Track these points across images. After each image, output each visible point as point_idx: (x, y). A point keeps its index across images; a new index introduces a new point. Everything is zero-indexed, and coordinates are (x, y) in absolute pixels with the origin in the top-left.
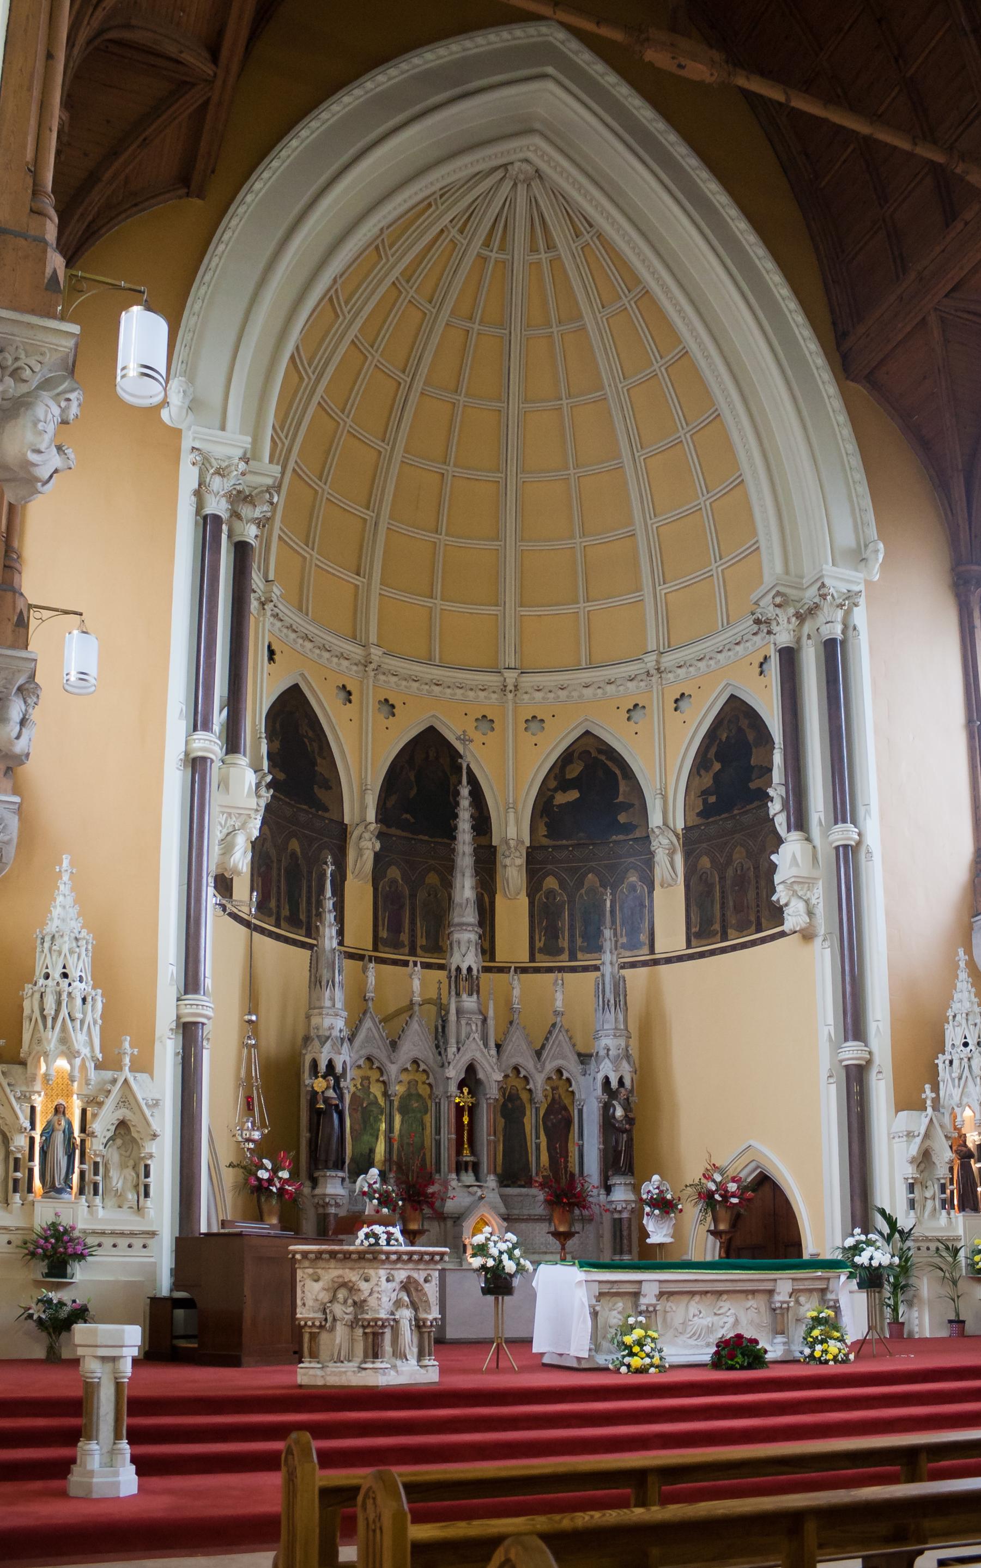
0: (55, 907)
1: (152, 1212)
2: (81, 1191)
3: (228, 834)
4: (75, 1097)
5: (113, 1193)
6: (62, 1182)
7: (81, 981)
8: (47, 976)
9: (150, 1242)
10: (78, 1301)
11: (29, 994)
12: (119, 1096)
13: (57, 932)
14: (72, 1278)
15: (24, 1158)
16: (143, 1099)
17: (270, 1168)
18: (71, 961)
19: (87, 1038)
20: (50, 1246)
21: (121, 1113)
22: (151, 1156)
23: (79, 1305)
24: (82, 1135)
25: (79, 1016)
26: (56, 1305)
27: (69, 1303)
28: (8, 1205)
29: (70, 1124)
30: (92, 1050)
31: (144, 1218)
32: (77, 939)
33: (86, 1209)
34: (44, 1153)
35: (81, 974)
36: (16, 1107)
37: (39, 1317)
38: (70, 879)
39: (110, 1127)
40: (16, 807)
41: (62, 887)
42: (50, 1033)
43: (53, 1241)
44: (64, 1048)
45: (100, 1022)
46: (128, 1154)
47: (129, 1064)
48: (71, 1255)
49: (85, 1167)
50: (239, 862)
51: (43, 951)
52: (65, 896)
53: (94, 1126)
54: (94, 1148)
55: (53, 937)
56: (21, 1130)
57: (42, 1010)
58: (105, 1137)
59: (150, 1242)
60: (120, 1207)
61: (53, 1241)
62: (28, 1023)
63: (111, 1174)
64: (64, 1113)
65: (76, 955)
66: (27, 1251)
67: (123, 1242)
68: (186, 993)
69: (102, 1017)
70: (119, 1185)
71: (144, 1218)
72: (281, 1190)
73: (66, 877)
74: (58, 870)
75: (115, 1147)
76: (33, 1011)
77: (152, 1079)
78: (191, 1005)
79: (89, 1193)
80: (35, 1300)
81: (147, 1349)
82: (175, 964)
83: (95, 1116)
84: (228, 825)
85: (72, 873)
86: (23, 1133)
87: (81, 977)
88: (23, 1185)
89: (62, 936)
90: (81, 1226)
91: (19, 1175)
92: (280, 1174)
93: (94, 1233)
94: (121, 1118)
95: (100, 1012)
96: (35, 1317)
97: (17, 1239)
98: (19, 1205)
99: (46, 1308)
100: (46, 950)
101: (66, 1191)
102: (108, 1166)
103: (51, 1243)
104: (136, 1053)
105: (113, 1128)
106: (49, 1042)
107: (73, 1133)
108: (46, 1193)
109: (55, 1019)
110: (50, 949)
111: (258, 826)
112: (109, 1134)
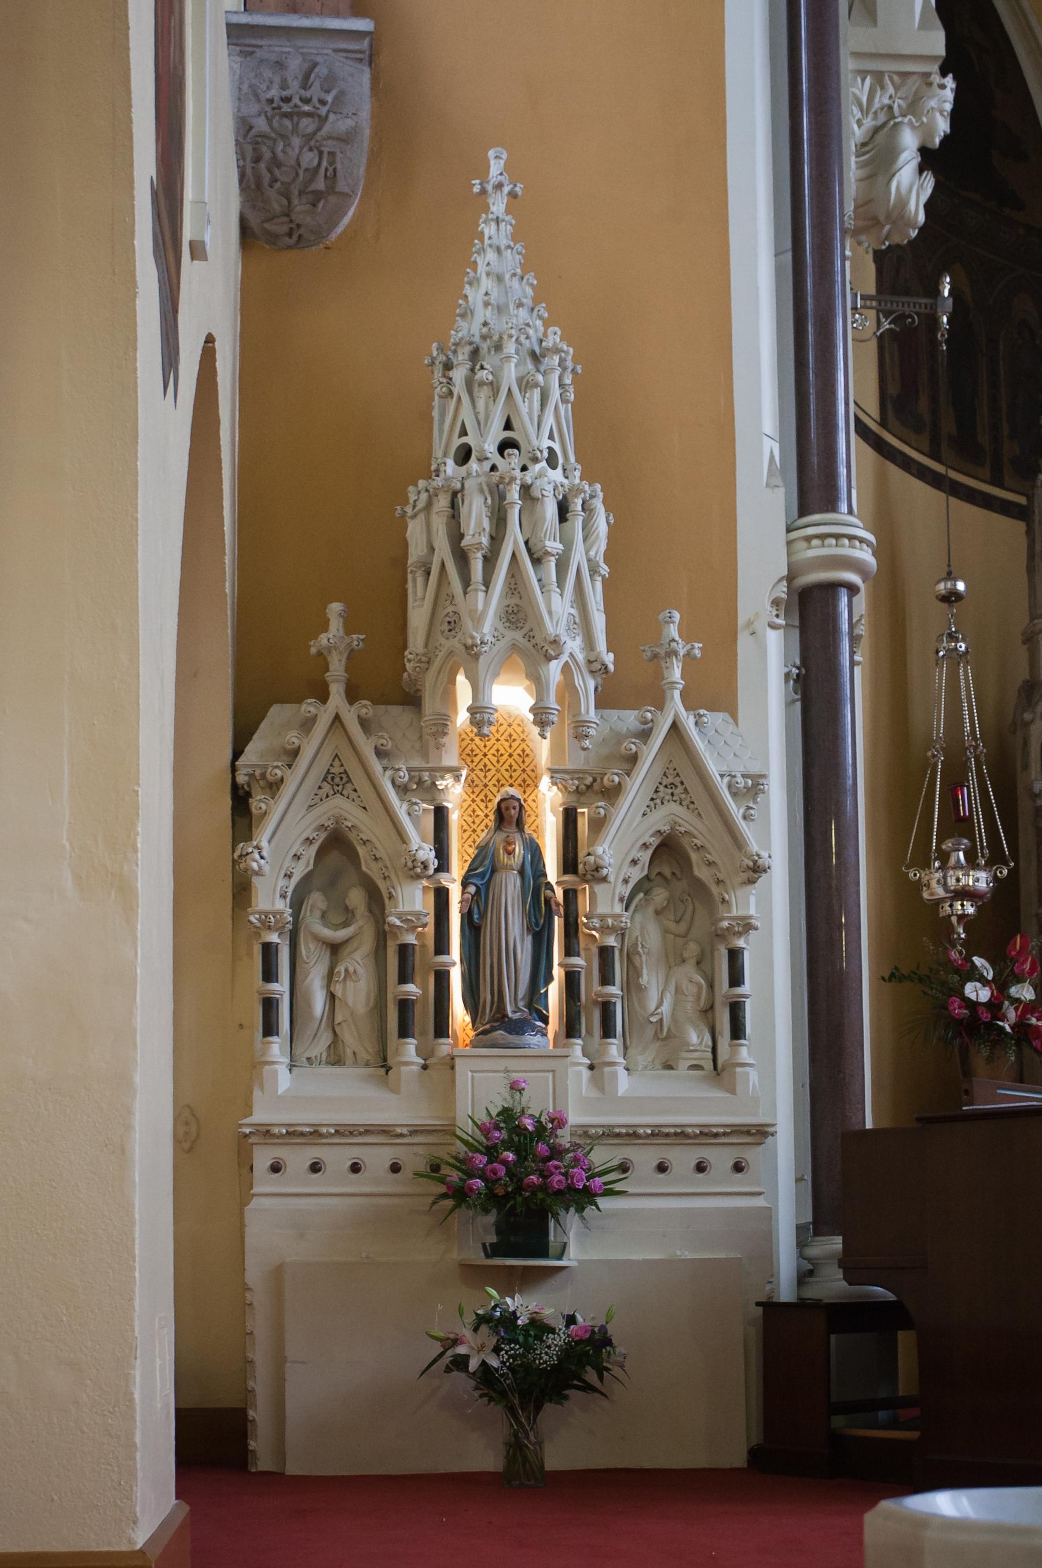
0: (474, 282)
1: (753, 1075)
2: (571, 1029)
3: (876, 130)
4: (545, 781)
5: (650, 1031)
6: (521, 1004)
7: (552, 461)
8: (464, 455)
9: (752, 1155)
10: (579, 1318)
11: (420, 505)
12: (658, 770)
13: (484, 337)
14: (560, 1258)
15: (423, 946)
16: (722, 776)
17: (990, 977)
18: (527, 407)
19: (573, 611)
20: (502, 1171)
21: (661, 819)
22: (747, 926)
23: (585, 1329)
24: (567, 878)
25: (554, 546)
26: (525, 1329)
27: (560, 1324)
28: (388, 1069)
29: (535, 852)
30: (589, 643)
31: (732, 1091)
32: (536, 358)
33: (586, 1073)
34: (472, 928)
35: (551, 444)
36: (400, 809)
37: (484, 1363)
38: (508, 211)
39: (635, 854)
40: (365, 44)
41: (489, 230)
42: (481, 595)
43: (510, 1156)
44: (518, 635)
45: (604, 569)
46: (682, 927)
47: (681, 684)
48: (559, 1193)
49: (578, 961)
50: (910, 191)
51: (451, 393)
52: (498, 250)
53: (600, 850)
54: (601, 909)
55: (475, 354)
56: (414, 871)
57: (456, 536)
58: (626, 881)
59: (752, 1155)
60: (669, 1067)
61: (510, 1156)
62: (420, 580)
63: (644, 980)
64: (520, 824)
65: (537, 393)
66: (442, 1189)
67: (682, 1158)
68: (803, 511)
69: (609, 557)
70: (666, 1008)
71: (732, 1091)
72: (1021, 1026)
73: (498, 205)
74: (476, 189)
75: (650, 910)
76: (432, 549)
77: (737, 724)
78: (823, 537)
79: (589, 1032)
80: (470, 1318)
81: (756, 1439)
82: (778, 439)
83: (598, 825)
84: (877, 105)
85: (512, 195)
86: (418, 877)
87: (551, 450)
88: (424, 1017)
89: (498, 347)
90: (575, 1118)
91: (412, 989)
92: (1013, 991)
93: (610, 1135)
94: (666, 828)
95: (603, 547)
96: (473, 1364)
97: (414, 1158)
98: (415, 1068)
99: (502, 1340)
100: (459, 387)
101: (534, 1028)
102: (636, 960)
103: (505, 1162)
104: (697, 653)
105: (646, 856)
106: (478, 620)
107: (545, 875)
108: (485, 1033)
109: (490, 561)
110: (469, 384)
111: (948, 107)
112: (636, 874)
